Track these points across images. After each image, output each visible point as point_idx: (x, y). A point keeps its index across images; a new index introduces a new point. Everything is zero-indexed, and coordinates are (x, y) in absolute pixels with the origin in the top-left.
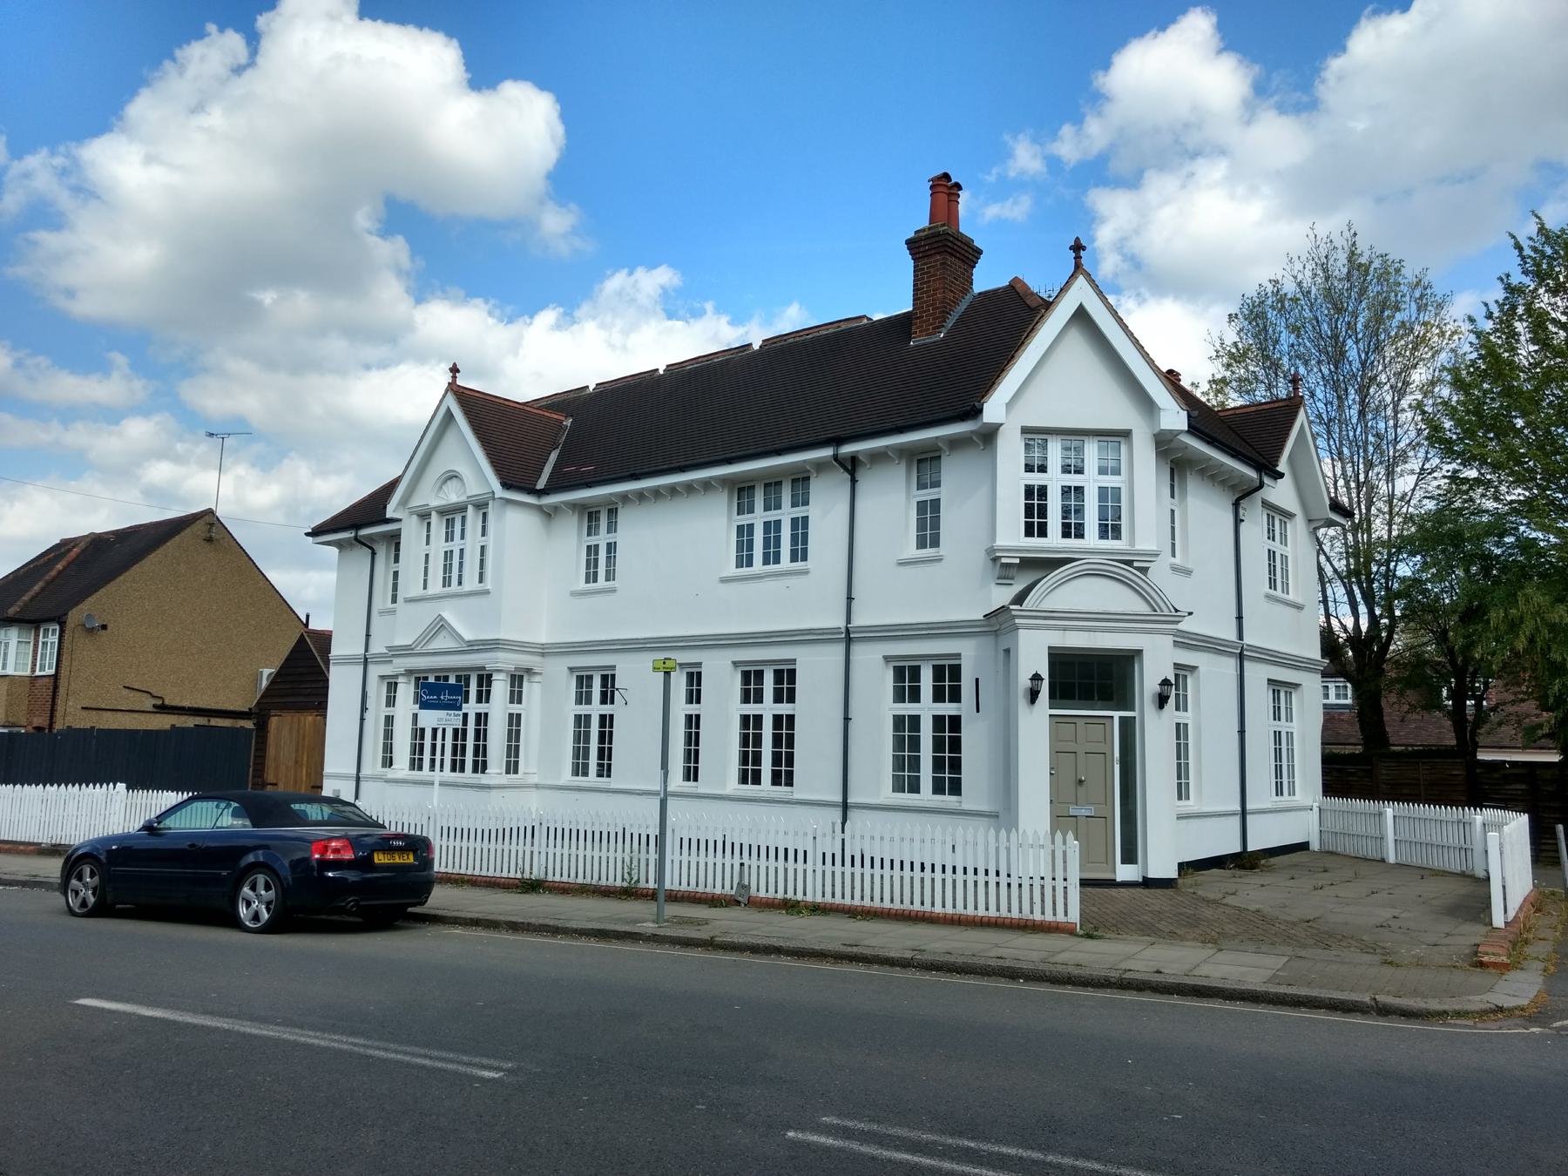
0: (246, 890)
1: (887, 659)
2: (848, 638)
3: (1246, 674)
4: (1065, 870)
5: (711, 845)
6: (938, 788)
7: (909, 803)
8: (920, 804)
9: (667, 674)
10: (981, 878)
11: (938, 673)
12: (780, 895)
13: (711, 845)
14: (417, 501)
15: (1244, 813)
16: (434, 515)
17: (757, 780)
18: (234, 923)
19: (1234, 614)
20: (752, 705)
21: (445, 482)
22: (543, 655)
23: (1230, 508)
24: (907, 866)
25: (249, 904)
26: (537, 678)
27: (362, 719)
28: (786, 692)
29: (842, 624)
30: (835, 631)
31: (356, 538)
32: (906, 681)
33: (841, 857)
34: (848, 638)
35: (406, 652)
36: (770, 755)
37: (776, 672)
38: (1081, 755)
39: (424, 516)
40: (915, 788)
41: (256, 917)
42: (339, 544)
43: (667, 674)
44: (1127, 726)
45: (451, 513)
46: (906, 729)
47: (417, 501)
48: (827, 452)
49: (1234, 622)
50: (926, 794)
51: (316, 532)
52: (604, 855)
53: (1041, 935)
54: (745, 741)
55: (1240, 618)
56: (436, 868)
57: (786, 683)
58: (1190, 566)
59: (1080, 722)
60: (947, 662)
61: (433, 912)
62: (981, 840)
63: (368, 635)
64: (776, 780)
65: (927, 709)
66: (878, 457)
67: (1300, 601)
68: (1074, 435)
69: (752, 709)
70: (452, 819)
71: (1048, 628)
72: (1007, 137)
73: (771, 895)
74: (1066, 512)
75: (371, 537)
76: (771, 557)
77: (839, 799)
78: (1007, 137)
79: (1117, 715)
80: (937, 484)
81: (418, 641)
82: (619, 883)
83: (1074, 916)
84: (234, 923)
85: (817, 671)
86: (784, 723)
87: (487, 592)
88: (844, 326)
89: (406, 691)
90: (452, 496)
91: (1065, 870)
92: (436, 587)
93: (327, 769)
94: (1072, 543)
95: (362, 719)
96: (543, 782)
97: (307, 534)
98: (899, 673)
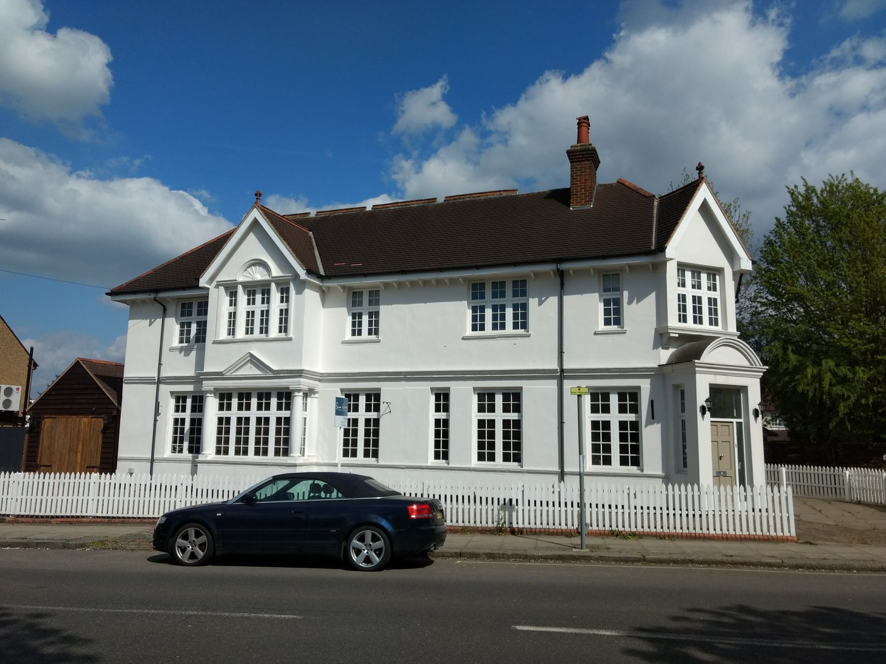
0: (355, 542)
1: (475, 389)
2: (561, 375)
4: (733, 505)
5: (123, 487)
6: (624, 462)
7: (284, 462)
9: (579, 396)
10: (620, 510)
12: (607, 528)
13: (123, 487)
14: (221, 277)
15: (152, 460)
16: (240, 289)
18: (350, 566)
20: (180, 413)
21: (254, 265)
22: (320, 381)
24: (538, 504)
25: (358, 552)
26: (317, 395)
27: (155, 421)
30: (555, 371)
31: (155, 299)
32: (486, 400)
35: (219, 376)
36: (504, 442)
38: (720, 442)
39: (231, 290)
40: (607, 461)
41: (367, 560)
42: (132, 304)
43: (579, 396)
45: (251, 289)
47: (221, 277)
50: (615, 465)
51: (113, 293)
53: (781, 544)
54: (219, 431)
56: (448, 523)
57: (513, 400)
61: (449, 550)
62: (683, 493)
63: (160, 364)
65: (499, 416)
66: (585, 272)
68: (697, 270)
69: (225, 414)
70: (443, 488)
72: (493, 107)
73: (601, 528)
74: (700, 312)
75: (164, 299)
76: (499, 324)
78: (493, 107)
79: (735, 420)
80: (617, 289)
81: (228, 370)
82: (490, 525)
83: (793, 533)
84: (350, 566)
87: (290, 339)
88: (504, 194)
89: (587, 400)
90: (258, 275)
91: (733, 505)
92: (240, 333)
93: (120, 454)
95: (155, 421)
96: (320, 461)
97: (107, 294)
98: (481, 397)
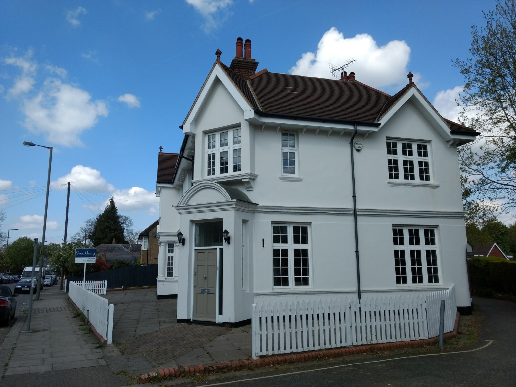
3: (358, 223)
7: (436, 287)
8: (439, 287)
11: (296, 230)
13: (406, 312)
17: (405, 281)
19: (352, 195)
23: (349, 145)
28: (430, 240)
29: (351, 206)
33: (359, 315)
34: (355, 213)
37: (409, 230)
40: (405, 281)
44: (221, 250)
46: (280, 256)
48: (350, 127)
49: (352, 199)
52: (393, 322)
55: (354, 197)
58: (301, 177)
59: (206, 252)
60: (300, 226)
64: (298, 282)
67: (436, 183)
71: (189, 213)
77: (355, 289)
79: (218, 247)
85: (319, 230)
86: (431, 254)
94: (237, 173)
